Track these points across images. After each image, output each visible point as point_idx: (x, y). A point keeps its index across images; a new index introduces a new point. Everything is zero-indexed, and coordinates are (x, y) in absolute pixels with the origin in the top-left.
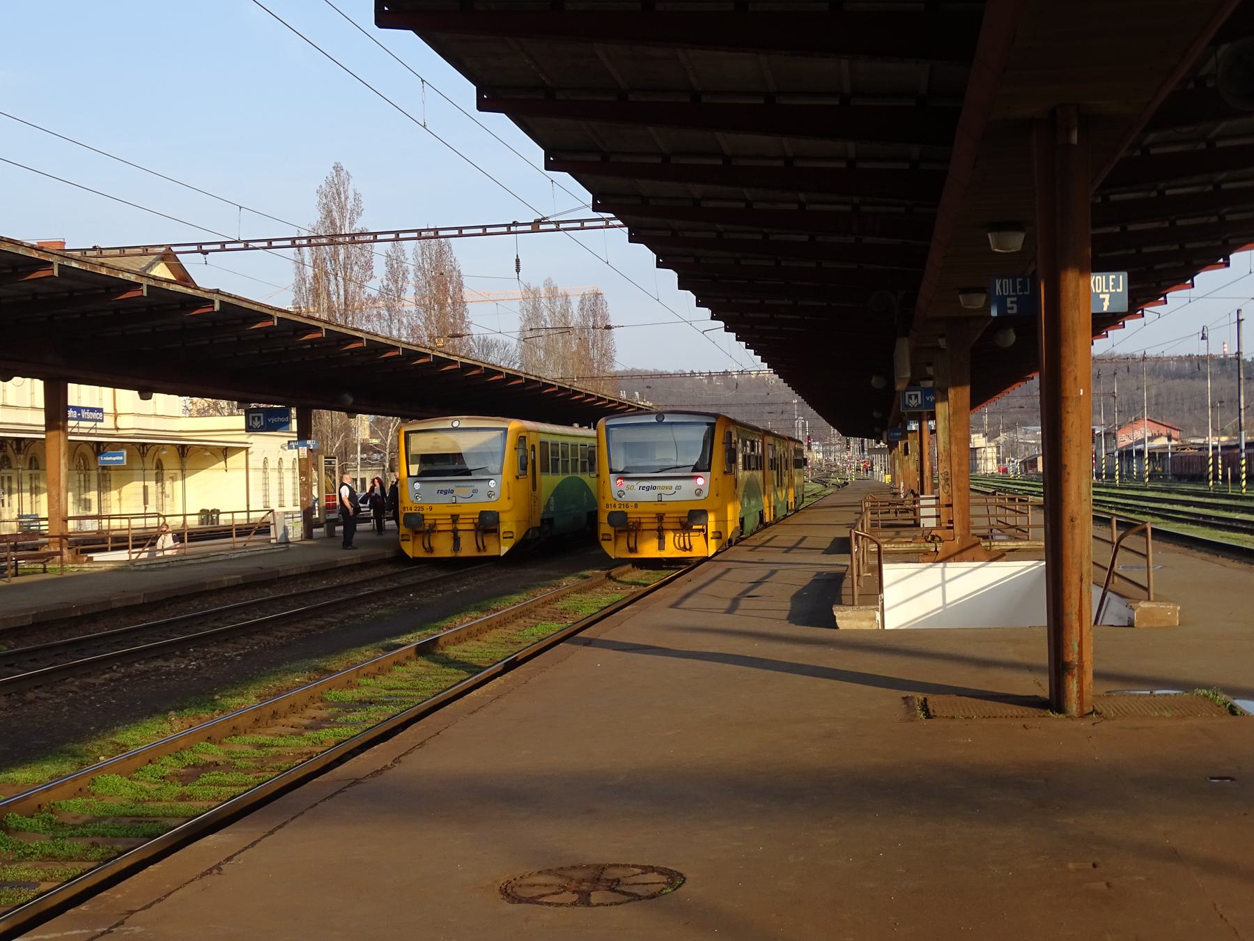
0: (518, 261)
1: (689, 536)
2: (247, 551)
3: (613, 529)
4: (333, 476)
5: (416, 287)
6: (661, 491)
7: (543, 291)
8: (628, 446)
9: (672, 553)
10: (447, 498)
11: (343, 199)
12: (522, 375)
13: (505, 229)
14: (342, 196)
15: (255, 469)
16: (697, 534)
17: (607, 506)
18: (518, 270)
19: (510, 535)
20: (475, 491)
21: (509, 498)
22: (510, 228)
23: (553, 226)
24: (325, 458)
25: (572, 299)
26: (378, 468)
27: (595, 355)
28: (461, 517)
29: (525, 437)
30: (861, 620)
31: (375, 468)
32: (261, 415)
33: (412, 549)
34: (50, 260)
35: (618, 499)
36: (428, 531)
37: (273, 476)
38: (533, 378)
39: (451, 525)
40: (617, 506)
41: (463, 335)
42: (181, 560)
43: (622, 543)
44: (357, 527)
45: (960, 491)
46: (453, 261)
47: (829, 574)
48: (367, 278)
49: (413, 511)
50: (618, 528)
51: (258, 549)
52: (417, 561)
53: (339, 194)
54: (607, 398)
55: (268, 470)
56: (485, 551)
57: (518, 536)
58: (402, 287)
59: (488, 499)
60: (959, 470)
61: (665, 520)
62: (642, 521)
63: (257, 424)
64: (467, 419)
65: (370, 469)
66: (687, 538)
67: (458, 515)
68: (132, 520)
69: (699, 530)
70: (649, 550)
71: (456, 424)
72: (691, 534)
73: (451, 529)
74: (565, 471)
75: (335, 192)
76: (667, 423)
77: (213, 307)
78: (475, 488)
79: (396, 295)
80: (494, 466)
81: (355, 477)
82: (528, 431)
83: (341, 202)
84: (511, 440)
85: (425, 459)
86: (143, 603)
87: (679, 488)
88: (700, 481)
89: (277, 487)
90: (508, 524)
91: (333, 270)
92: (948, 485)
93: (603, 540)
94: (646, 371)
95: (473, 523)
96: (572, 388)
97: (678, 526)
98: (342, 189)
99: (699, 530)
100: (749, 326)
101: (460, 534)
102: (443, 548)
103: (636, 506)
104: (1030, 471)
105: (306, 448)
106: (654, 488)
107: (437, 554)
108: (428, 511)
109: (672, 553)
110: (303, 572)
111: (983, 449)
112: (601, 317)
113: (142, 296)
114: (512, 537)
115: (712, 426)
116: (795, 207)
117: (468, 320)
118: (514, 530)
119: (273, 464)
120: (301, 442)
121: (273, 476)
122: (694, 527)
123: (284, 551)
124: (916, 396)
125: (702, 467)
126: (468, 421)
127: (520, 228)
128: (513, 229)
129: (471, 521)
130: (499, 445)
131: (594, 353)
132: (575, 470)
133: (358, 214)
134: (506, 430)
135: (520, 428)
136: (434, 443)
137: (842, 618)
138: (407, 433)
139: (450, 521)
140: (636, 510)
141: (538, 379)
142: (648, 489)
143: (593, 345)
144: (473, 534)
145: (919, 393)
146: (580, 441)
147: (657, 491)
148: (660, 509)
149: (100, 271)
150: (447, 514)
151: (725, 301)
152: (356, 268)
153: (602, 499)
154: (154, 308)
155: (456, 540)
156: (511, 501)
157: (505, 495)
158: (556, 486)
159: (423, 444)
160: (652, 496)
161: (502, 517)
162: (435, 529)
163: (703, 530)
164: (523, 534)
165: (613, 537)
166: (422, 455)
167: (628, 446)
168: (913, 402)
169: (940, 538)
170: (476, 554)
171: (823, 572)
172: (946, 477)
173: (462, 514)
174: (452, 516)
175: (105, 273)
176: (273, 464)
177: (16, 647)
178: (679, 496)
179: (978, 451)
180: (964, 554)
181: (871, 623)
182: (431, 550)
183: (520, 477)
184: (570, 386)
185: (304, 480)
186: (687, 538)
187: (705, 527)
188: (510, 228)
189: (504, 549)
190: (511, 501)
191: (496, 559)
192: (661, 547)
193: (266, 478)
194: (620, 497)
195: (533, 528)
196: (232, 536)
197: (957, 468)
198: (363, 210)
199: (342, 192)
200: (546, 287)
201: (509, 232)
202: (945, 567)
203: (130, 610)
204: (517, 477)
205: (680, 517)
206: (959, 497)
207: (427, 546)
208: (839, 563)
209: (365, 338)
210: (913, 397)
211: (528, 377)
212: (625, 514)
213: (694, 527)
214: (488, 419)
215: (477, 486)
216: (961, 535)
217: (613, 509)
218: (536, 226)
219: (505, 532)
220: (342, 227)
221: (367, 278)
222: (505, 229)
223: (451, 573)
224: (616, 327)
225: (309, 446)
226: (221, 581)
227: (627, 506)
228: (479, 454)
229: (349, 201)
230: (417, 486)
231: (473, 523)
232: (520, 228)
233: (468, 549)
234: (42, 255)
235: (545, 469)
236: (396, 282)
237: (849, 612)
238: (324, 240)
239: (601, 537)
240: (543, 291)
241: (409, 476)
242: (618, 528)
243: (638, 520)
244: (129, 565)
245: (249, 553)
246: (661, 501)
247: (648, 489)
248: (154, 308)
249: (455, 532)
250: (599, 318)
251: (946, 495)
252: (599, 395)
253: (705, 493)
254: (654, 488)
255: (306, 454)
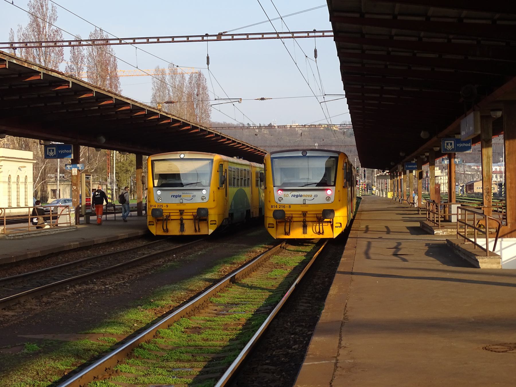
0: (208, 58)
1: (322, 225)
2: (58, 230)
3: (275, 220)
4: (89, 187)
5: (88, 67)
6: (305, 198)
7: (167, 71)
8: (282, 170)
9: (311, 236)
10: (177, 200)
11: (45, 10)
12: (199, 127)
13: (200, 38)
14: (44, 8)
15: (4, 182)
16: (326, 224)
17: (272, 206)
18: (208, 63)
19: (215, 222)
20: (194, 196)
21: (214, 201)
22: (204, 38)
23: (230, 37)
24: (86, 175)
25: (186, 75)
26: (68, 183)
27: (198, 112)
28: (185, 211)
29: (222, 164)
30: (492, 264)
31: (66, 183)
32: (55, 148)
33: (155, 230)
34: (5, 59)
35: (279, 202)
36: (165, 220)
37: (22, 187)
38: (204, 128)
39: (179, 216)
40: (278, 207)
41: (174, 102)
42: (29, 234)
43: (281, 229)
44: (90, 218)
45: (511, 198)
46: (111, 50)
47: (432, 244)
48: (60, 61)
49: (156, 208)
50: (278, 220)
51: (63, 229)
52: (159, 237)
53: (42, 6)
54: (237, 141)
55: (11, 183)
56: (199, 232)
57: (218, 223)
58: (80, 67)
59: (202, 201)
60: (510, 186)
61: (307, 215)
62: (294, 216)
63: (51, 154)
64: (189, 153)
65: (63, 183)
66: (321, 227)
67: (184, 210)
68: (6, 209)
69: (328, 222)
70: (297, 234)
71: (182, 156)
72: (324, 224)
73: (179, 218)
74: (238, 186)
75: (40, 5)
76: (309, 157)
77: (69, 86)
78: (194, 194)
79: (77, 72)
80: (205, 181)
81: (55, 188)
82: (224, 161)
83: (43, 12)
84: (215, 166)
85: (162, 176)
86: (40, 256)
87: (316, 196)
88: (329, 192)
89: (15, 193)
90: (213, 216)
91: (38, 55)
92: (489, 195)
93: (269, 227)
94: (219, 124)
95: (193, 215)
96: (221, 135)
97: (315, 219)
98: (44, 3)
99: (328, 222)
100: (365, 101)
101: (184, 221)
102: (174, 229)
103: (290, 207)
104: (469, 192)
105: (76, 169)
106: (301, 196)
107: (170, 233)
108: (166, 208)
109: (311, 236)
110: (104, 242)
111: (439, 177)
112: (202, 88)
113: (6, 68)
114: (216, 224)
115: (337, 158)
116: (446, 41)
117: (120, 89)
118: (216, 220)
119: (14, 179)
120: (74, 165)
121: (22, 187)
122: (326, 220)
123: (74, 231)
124: (451, 144)
125: (324, 184)
126: (189, 154)
127: (209, 38)
128: (205, 38)
129: (192, 214)
130: (208, 169)
131: (197, 111)
132: (241, 185)
133: (54, 20)
134: (212, 160)
135: (221, 159)
136: (169, 167)
137: (482, 263)
138: (153, 161)
139: (179, 214)
140: (289, 209)
141: (206, 129)
142: (297, 196)
143: (197, 107)
144: (192, 221)
145: (453, 142)
146: (244, 168)
147: (303, 198)
148: (305, 209)
149: (25, 65)
150: (177, 210)
151: (360, 87)
152: (52, 55)
153: (268, 202)
154: (33, 86)
155: (182, 225)
156: (215, 202)
157: (212, 199)
158: (235, 192)
159: (162, 168)
160: (300, 201)
161: (211, 212)
162: (169, 218)
163: (330, 222)
164: (221, 223)
165: (275, 226)
166: (160, 174)
167: (282, 170)
168: (449, 147)
169: (484, 226)
170: (194, 234)
171: (430, 243)
172: (488, 191)
173: (187, 210)
174: (180, 210)
175: (26, 66)
176: (14, 179)
177: (27, 272)
178: (316, 201)
179: (436, 178)
180: (513, 233)
181: (498, 265)
182: (167, 231)
183: (220, 188)
184: (220, 133)
185: (75, 188)
186: (321, 227)
187: (331, 220)
188: (204, 38)
189: (211, 231)
190: (215, 202)
191: (206, 238)
192: (305, 232)
193: (9, 188)
194: (280, 201)
195: (225, 219)
196: (50, 219)
197: (509, 185)
198: (57, 17)
199: (44, 5)
200: (170, 68)
201: (203, 40)
202: (502, 241)
203: (34, 260)
204: (219, 188)
205: (316, 214)
206: (511, 201)
207: (165, 228)
208: (432, 239)
209: (131, 103)
210: (449, 144)
211: (202, 128)
212: (283, 211)
213: (326, 220)
214: (201, 154)
215: (195, 193)
216: (511, 223)
217: (276, 209)
218: (219, 37)
219: (211, 221)
220: (44, 28)
221: (60, 61)
222: (200, 38)
223: (186, 244)
224: (267, 99)
225: (78, 168)
226: (71, 245)
227: (284, 207)
228: (196, 174)
229: (49, 11)
230: (159, 193)
231: (193, 215)
232: (209, 38)
233: (189, 230)
234: (2, 56)
235: (230, 184)
236: (77, 64)
237: (486, 259)
238: (84, 43)
239: (267, 226)
240: (167, 71)
241: (154, 186)
242: (278, 220)
243: (291, 215)
244: (5, 236)
245: (59, 231)
246: (305, 204)
247: (297, 196)
248: (33, 86)
249: (182, 220)
250: (201, 89)
251: (487, 201)
252: (233, 139)
253: (332, 199)
254: (301, 196)
255: (76, 173)
